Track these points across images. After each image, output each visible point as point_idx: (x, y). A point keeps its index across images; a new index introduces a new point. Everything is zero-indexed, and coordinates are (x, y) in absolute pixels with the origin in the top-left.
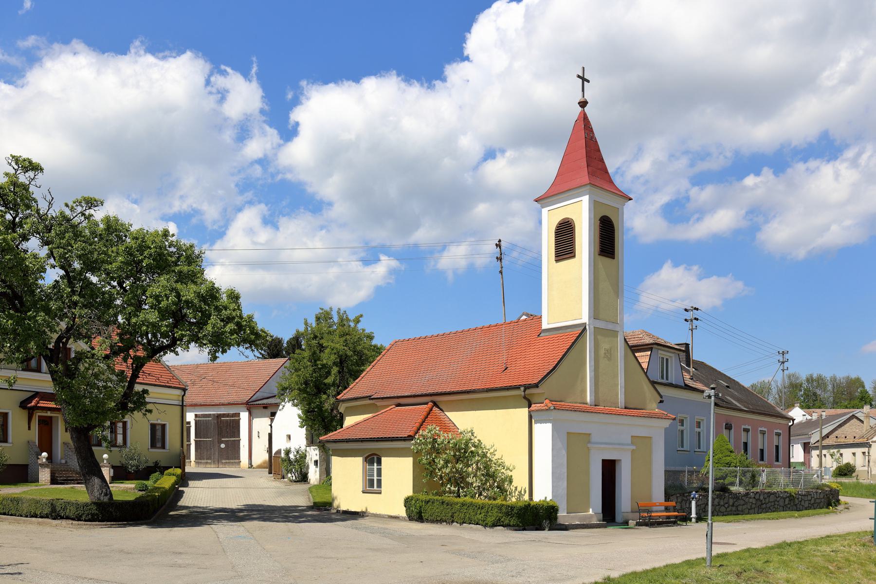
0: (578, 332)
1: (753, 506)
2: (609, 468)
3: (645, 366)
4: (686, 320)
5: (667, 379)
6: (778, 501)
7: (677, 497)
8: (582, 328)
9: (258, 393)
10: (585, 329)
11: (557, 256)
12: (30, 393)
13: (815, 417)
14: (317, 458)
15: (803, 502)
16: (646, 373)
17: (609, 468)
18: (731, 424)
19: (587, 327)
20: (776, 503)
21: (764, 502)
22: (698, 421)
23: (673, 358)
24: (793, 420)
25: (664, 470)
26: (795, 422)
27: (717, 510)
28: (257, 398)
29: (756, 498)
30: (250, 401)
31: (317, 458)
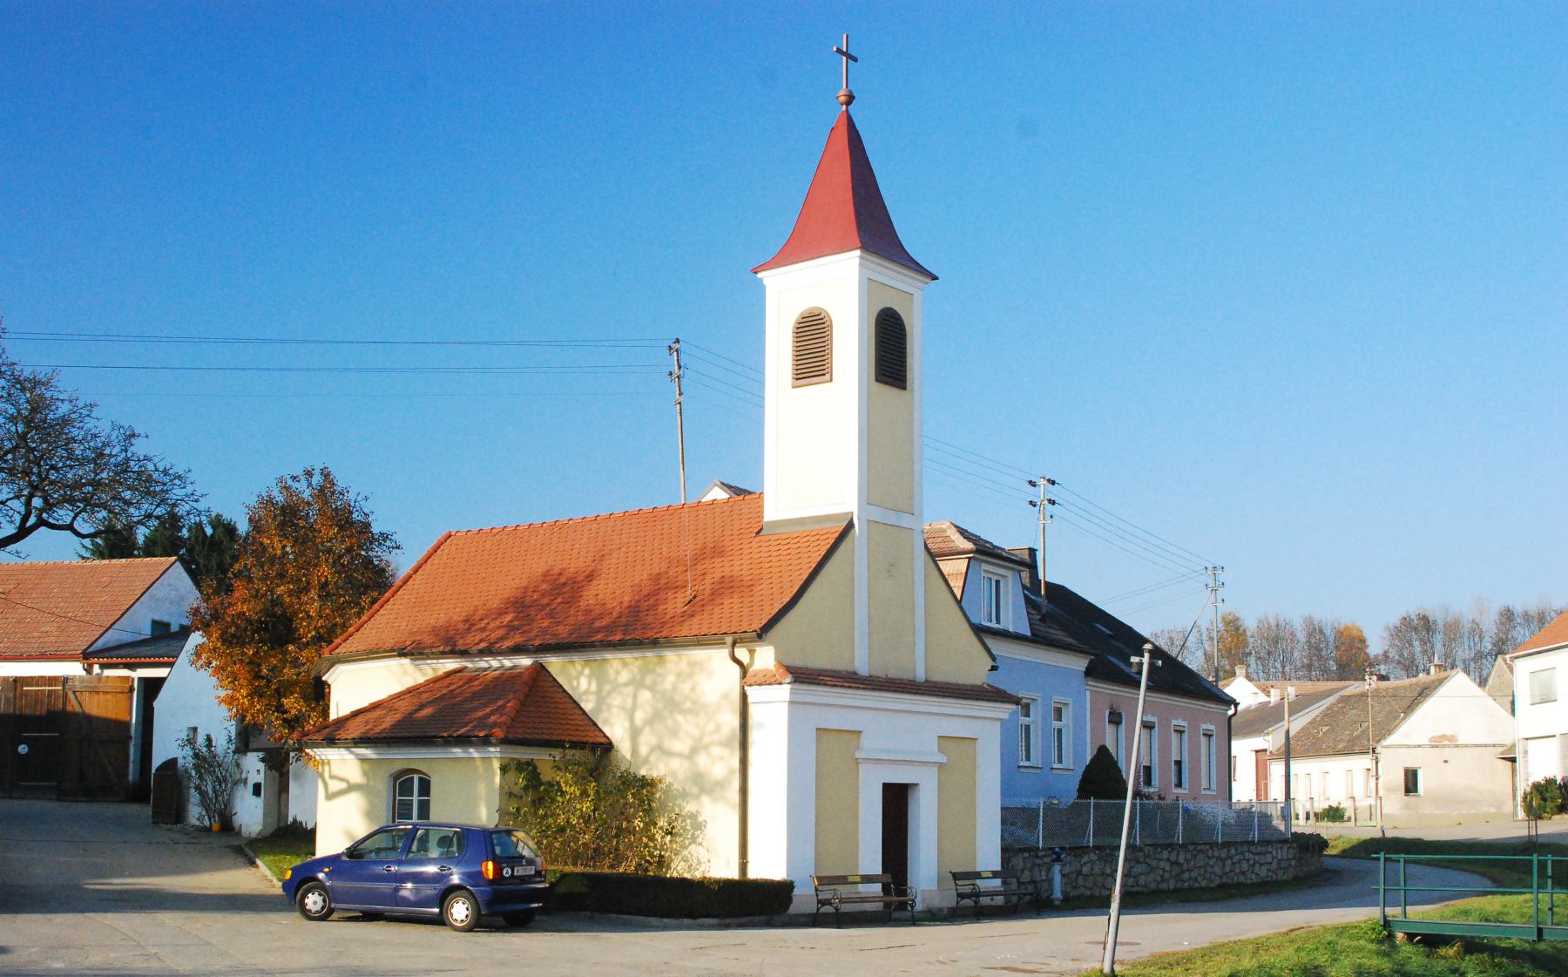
0: (837, 529)
1: (1167, 875)
2: (897, 799)
3: (957, 585)
4: (1033, 504)
5: (998, 621)
6: (1212, 866)
7: (1024, 858)
8: (844, 524)
9: (110, 631)
10: (850, 525)
11: (797, 379)
12: (1115, 751)
13: (1275, 696)
14: (260, 779)
15: (1257, 866)
16: (959, 602)
17: (897, 799)
18: (1120, 714)
19: (856, 521)
20: (1210, 870)
21: (1185, 867)
22: (1058, 706)
23: (1010, 578)
24: (1236, 706)
25: (1000, 807)
26: (1239, 708)
27: (1100, 885)
28: (104, 644)
29: (1171, 859)
30: (90, 650)
31: (260, 779)
